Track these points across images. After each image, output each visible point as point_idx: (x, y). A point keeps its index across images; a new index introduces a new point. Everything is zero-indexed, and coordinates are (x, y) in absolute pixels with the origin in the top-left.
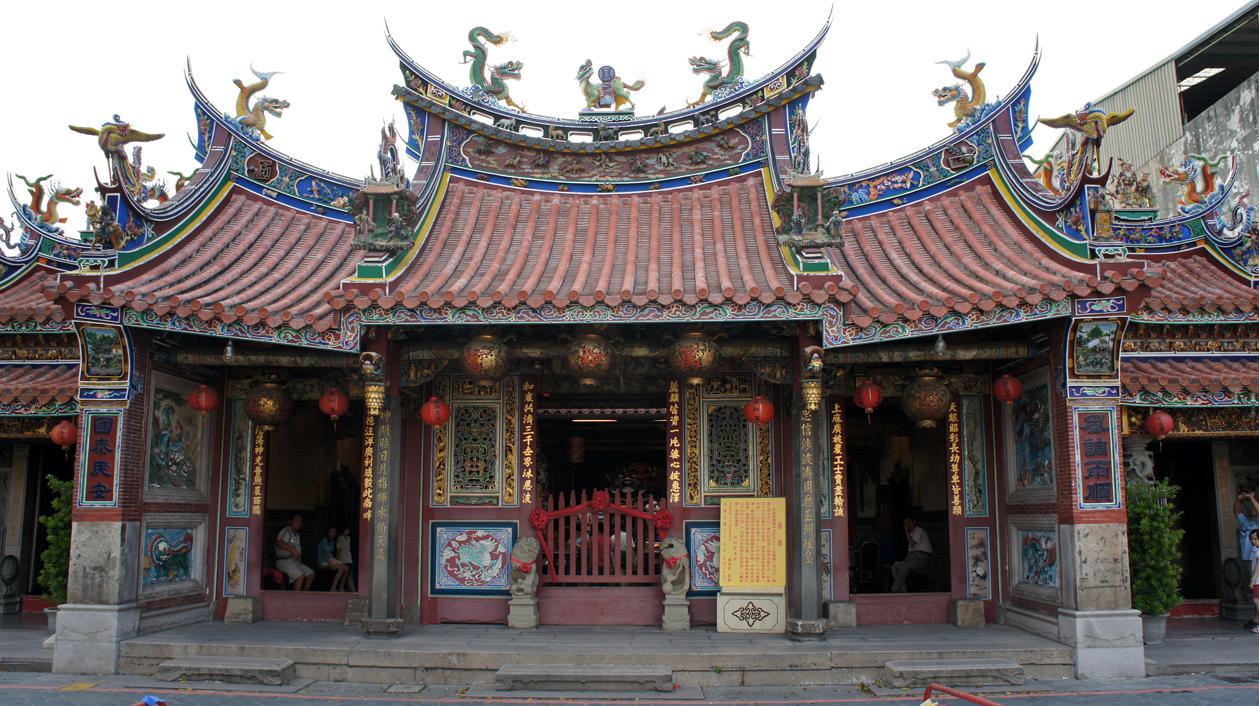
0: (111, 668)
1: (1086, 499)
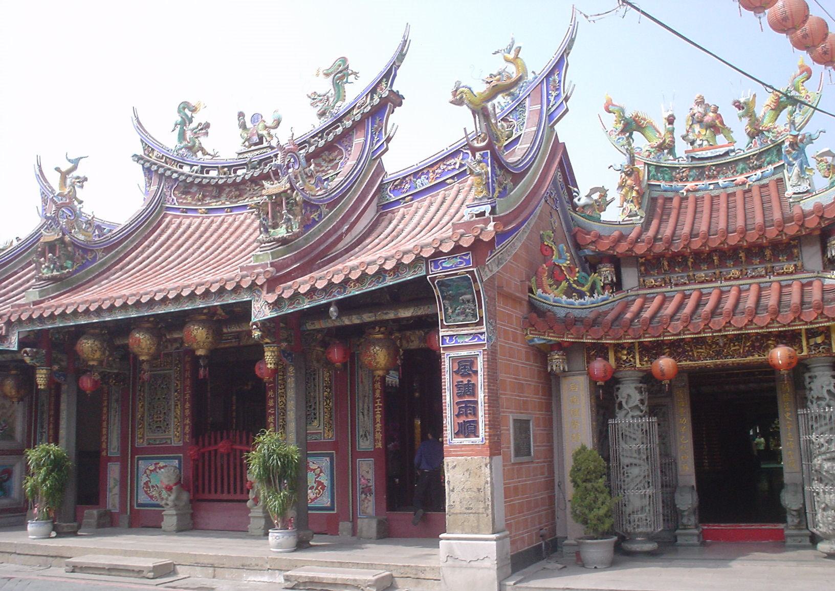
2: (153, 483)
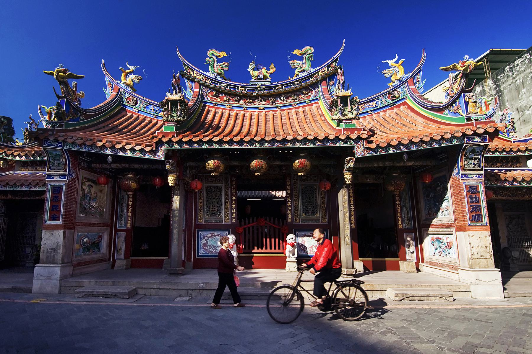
0: (57, 291)
1: (472, 221)
2: (210, 243)
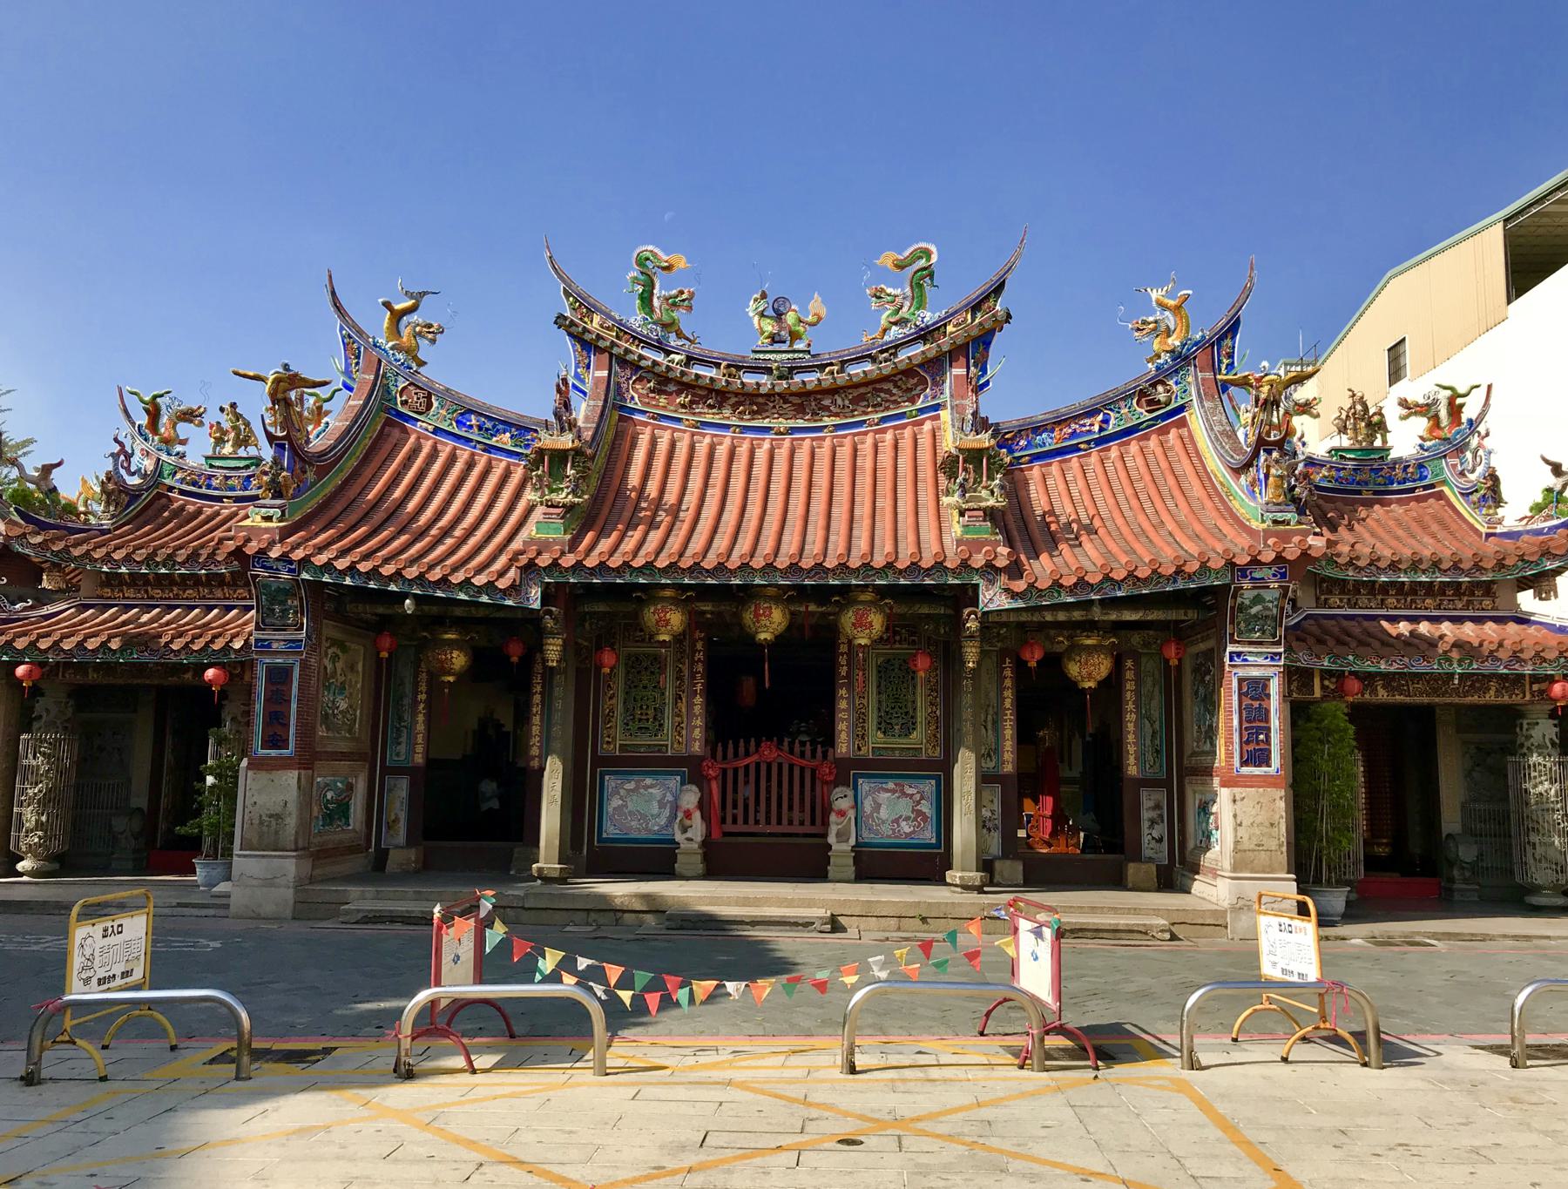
2: (631, 806)
